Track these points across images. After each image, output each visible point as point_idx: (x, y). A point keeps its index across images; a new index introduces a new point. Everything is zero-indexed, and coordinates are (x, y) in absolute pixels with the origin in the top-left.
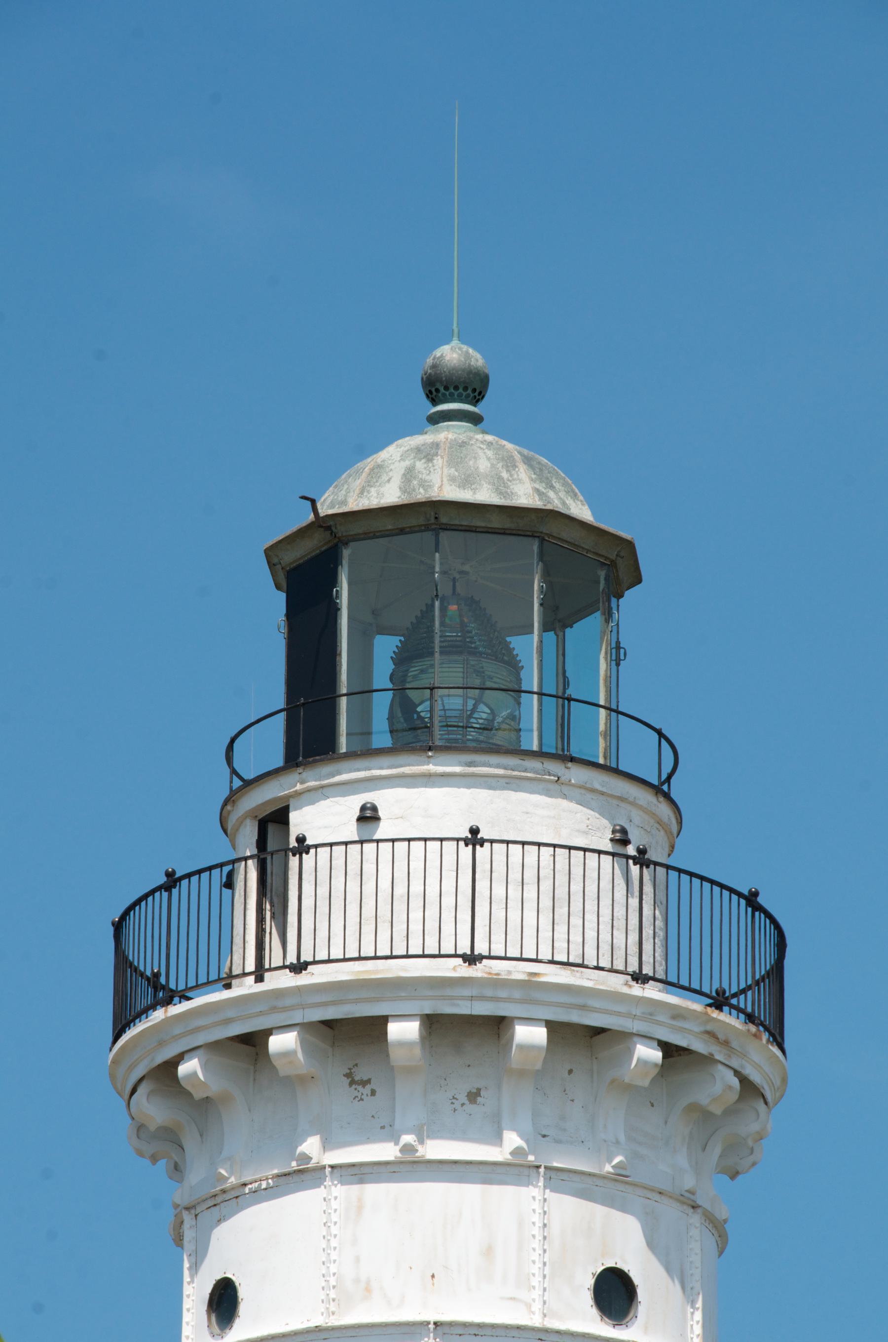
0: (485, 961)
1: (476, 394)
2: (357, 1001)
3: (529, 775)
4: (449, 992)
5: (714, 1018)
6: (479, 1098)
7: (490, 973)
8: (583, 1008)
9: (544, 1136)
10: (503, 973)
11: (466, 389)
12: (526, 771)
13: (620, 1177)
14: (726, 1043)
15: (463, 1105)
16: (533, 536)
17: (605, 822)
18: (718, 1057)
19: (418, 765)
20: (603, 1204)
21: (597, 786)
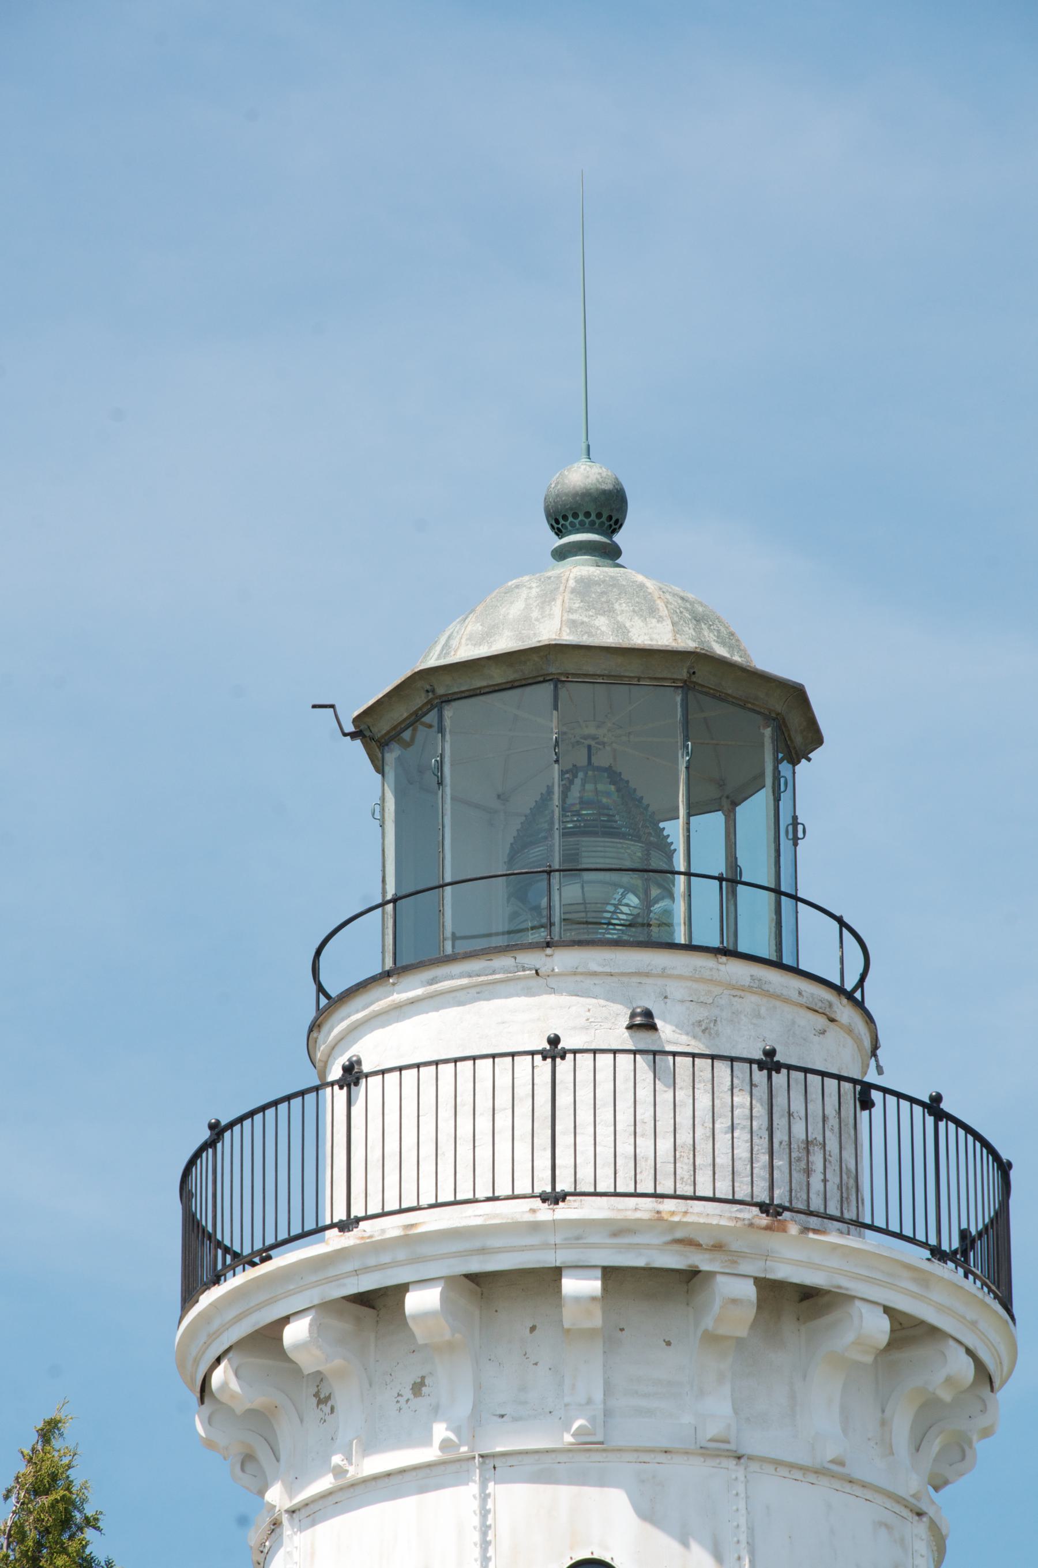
0: (362, 1225)
1: (612, 522)
2: (259, 1307)
3: (497, 976)
4: (332, 1272)
5: (679, 1223)
6: (424, 1389)
7: (362, 1238)
8: (483, 1251)
9: (502, 1416)
10: (376, 1234)
11: (575, 515)
12: (494, 972)
13: (589, 1445)
14: (718, 1247)
15: (408, 1401)
16: (544, 681)
17: (625, 1010)
18: (705, 1267)
19: (386, 998)
20: (570, 1483)
21: (594, 967)
